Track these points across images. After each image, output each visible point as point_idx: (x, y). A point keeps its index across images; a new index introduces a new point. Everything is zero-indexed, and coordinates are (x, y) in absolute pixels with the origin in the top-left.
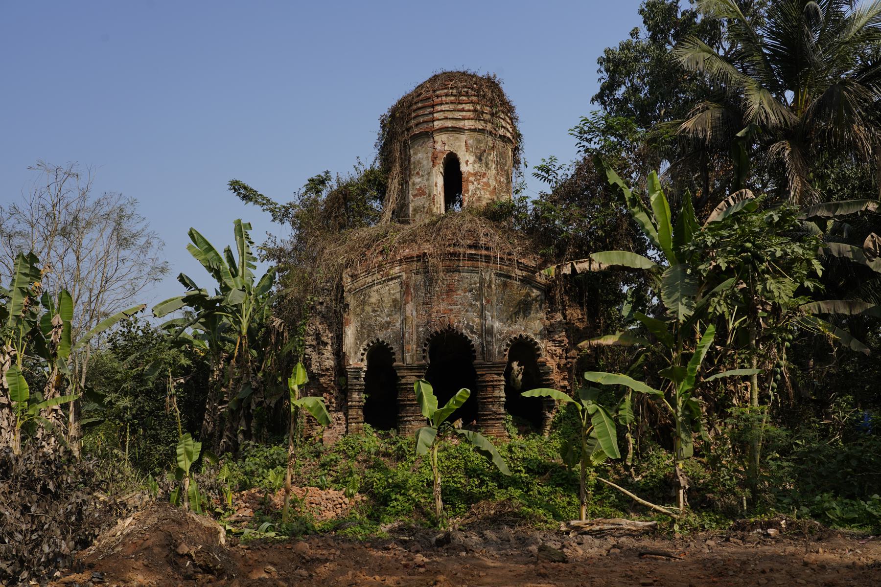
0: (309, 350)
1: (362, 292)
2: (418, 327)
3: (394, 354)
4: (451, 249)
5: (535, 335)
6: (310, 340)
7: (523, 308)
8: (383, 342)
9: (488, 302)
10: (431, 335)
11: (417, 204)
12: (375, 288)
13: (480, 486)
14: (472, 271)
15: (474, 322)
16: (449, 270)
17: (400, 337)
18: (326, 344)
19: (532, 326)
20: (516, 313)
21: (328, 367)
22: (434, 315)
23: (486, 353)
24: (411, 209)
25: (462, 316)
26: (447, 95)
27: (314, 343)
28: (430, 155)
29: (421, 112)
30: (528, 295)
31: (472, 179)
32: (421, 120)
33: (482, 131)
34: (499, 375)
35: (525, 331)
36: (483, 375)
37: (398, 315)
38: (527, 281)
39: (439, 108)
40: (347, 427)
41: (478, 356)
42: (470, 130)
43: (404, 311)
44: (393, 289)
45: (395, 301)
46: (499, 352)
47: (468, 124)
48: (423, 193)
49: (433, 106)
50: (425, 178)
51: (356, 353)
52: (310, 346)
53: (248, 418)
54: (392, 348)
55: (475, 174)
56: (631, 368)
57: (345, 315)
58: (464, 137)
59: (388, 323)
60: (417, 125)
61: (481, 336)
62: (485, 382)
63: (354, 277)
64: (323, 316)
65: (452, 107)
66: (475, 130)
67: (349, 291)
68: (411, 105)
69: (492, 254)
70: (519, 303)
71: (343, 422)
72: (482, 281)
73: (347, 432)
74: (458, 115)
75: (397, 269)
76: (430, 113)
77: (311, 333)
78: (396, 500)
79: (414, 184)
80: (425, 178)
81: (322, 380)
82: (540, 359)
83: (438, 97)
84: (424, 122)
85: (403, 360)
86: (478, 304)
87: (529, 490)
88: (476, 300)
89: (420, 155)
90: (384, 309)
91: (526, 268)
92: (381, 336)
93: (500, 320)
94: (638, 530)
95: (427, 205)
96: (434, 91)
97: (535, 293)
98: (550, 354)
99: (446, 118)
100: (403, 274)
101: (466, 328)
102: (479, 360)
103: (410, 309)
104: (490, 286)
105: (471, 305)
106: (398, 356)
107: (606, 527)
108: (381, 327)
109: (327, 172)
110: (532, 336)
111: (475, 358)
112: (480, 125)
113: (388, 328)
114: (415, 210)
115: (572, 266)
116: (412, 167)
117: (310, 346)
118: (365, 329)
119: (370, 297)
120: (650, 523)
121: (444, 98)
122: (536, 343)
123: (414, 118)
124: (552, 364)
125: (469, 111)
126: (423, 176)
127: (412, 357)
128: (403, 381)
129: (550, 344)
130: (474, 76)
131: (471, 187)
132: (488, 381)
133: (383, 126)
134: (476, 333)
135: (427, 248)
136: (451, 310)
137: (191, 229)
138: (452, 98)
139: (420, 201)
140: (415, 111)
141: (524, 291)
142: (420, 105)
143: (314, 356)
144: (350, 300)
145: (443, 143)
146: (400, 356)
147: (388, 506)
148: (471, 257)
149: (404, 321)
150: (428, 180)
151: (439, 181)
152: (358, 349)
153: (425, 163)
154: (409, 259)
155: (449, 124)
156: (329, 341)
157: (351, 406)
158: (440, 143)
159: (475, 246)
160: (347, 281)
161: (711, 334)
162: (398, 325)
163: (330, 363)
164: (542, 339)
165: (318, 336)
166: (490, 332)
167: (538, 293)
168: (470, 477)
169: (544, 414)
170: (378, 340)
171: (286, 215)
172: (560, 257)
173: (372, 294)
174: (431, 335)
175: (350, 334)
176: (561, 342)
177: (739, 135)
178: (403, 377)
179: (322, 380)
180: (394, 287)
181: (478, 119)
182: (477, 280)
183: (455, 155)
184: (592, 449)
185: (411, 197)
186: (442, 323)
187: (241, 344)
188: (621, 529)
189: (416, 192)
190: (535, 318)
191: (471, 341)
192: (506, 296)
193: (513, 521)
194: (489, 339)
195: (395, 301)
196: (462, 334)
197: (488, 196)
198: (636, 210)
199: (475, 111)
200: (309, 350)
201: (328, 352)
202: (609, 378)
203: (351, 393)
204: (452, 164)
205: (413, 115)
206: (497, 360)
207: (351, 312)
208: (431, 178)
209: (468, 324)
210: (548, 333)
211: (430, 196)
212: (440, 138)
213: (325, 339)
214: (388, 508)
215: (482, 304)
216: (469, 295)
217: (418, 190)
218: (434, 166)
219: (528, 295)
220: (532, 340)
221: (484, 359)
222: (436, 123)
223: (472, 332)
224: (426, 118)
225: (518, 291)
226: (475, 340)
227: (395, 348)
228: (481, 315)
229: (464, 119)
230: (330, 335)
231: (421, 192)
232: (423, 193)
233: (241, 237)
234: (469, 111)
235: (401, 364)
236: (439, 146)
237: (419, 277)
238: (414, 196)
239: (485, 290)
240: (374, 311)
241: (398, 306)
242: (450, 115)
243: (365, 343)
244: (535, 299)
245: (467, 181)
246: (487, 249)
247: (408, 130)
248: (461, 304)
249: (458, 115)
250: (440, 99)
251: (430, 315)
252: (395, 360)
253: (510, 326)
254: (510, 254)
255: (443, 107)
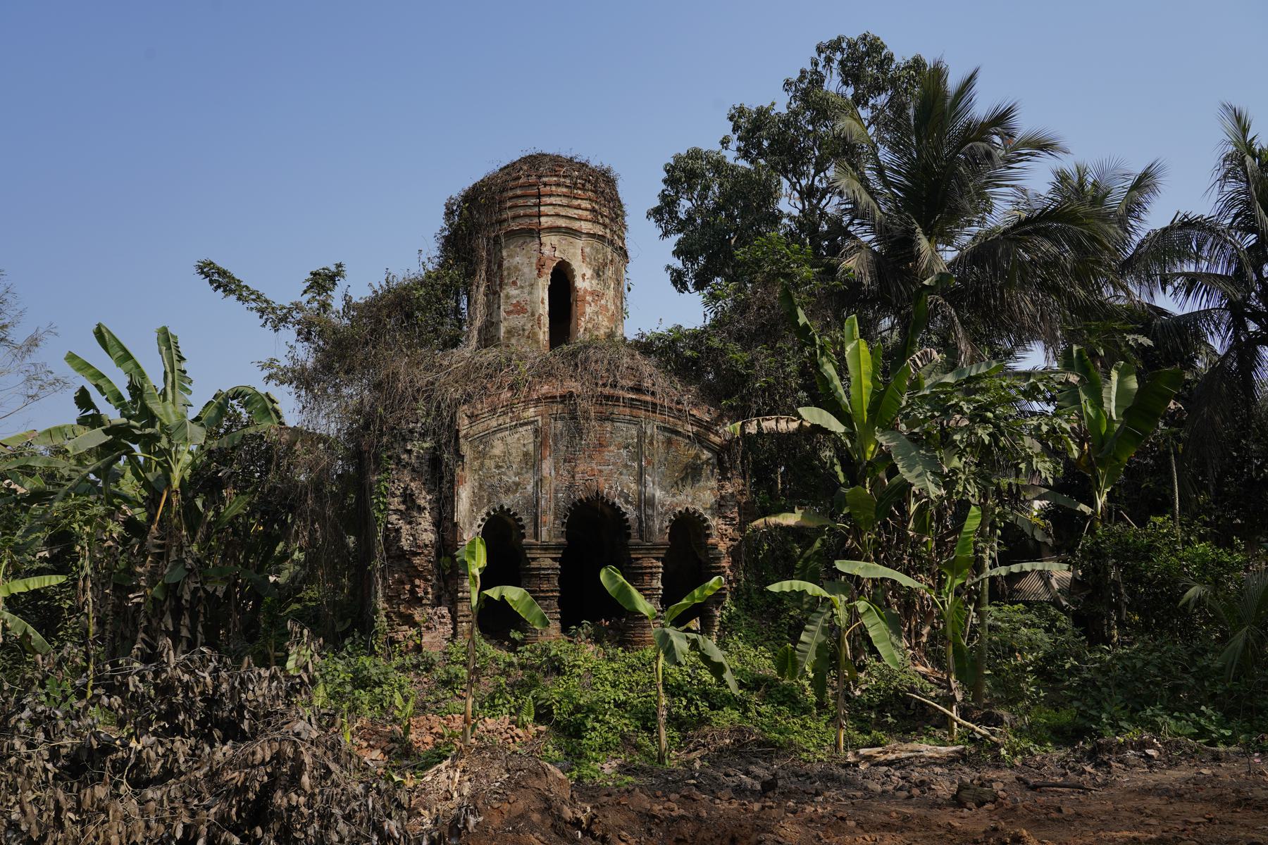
0: (393, 518)
1: (485, 438)
2: (556, 491)
3: (523, 527)
4: (607, 391)
5: (705, 509)
6: (395, 503)
7: (692, 473)
8: (509, 510)
9: (649, 463)
10: (574, 504)
11: (512, 324)
12: (499, 435)
13: (686, 707)
14: (629, 422)
15: (629, 488)
16: (603, 418)
17: (534, 505)
18: (421, 509)
19: (701, 497)
20: (682, 479)
21: (427, 542)
22: (578, 476)
23: (644, 531)
24: (503, 330)
25: (613, 478)
26: (558, 185)
27: (402, 507)
28: (534, 261)
29: (521, 202)
30: (697, 457)
31: (589, 298)
32: (522, 212)
33: (601, 238)
34: (657, 559)
35: (692, 503)
36: (638, 559)
37: (530, 474)
38: (700, 440)
39: (548, 200)
40: (454, 628)
41: (634, 534)
42: (588, 234)
43: (539, 469)
44: (523, 439)
45: (526, 454)
46: (661, 530)
47: (586, 227)
48: (523, 311)
49: (539, 196)
50: (526, 290)
51: (471, 525)
52: (396, 511)
53: (177, 614)
54: (520, 519)
55: (592, 293)
56: (805, 555)
57: (458, 471)
58: (580, 243)
59: (517, 484)
60: (514, 218)
61: (638, 507)
62: (641, 568)
63: (473, 417)
64: (413, 470)
65: (565, 201)
66: (593, 236)
67: (466, 437)
68: (504, 190)
69: (658, 402)
70: (686, 468)
71: (448, 620)
72: (641, 435)
73: (455, 635)
74: (571, 212)
75: (531, 411)
76: (535, 205)
77: (398, 493)
78: (594, 729)
79: (508, 297)
80: (526, 290)
81: (416, 561)
82: (711, 541)
83: (545, 185)
84: (525, 216)
85: (536, 536)
86: (635, 465)
87: (747, 710)
88: (634, 460)
89: (519, 259)
90: (509, 464)
91: (698, 422)
92: (507, 501)
93: (663, 488)
94: (941, 758)
95: (528, 326)
96: (540, 177)
97: (706, 455)
98: (721, 533)
99: (557, 215)
100: (539, 418)
101: (620, 495)
102: (634, 539)
103: (547, 467)
104: (651, 443)
105: (626, 466)
106: (529, 531)
107: (903, 755)
108: (508, 491)
109: (339, 266)
110: (701, 511)
111: (629, 536)
112: (599, 230)
113: (516, 491)
114: (510, 332)
115: (759, 424)
116: (505, 273)
117: (396, 511)
118: (485, 491)
119: (492, 447)
120: (954, 748)
121: (554, 188)
122: (705, 520)
123: (510, 208)
124: (723, 547)
125: (586, 209)
126: (522, 287)
127: (549, 531)
128: (534, 565)
129: (721, 521)
130: (583, 165)
131: (589, 310)
132: (646, 568)
133: (449, 213)
134: (631, 504)
135: (574, 386)
136: (601, 471)
137: (99, 326)
138: (565, 190)
139: (517, 321)
140: (511, 198)
141: (692, 452)
142: (519, 192)
143: (405, 529)
144: (466, 449)
145: (554, 247)
146: (532, 531)
147: (582, 738)
148: (631, 404)
149: (539, 483)
150: (530, 293)
151: (543, 293)
152: (475, 518)
153: (526, 270)
154: (551, 399)
155: (562, 223)
156: (428, 507)
157: (462, 598)
158: (549, 247)
159: (637, 389)
160: (464, 424)
161: (976, 517)
162: (530, 488)
163: (429, 537)
164: (713, 514)
165: (408, 498)
166: (650, 502)
167: (710, 455)
168: (673, 695)
169: (711, 611)
170: (502, 507)
171: (284, 319)
172: (742, 414)
173: (496, 443)
174: (574, 504)
175: (464, 496)
176: (733, 519)
177: (926, 282)
178: (534, 559)
179: (416, 561)
180: (526, 433)
181: (595, 222)
182: (635, 433)
183: (569, 265)
184: (805, 657)
185: (503, 314)
186: (588, 488)
187: (168, 500)
188: (921, 757)
189: (511, 308)
190: (706, 488)
191: (625, 514)
192: (670, 457)
193: (769, 752)
194: (650, 512)
195: (526, 454)
196: (614, 504)
197: (606, 323)
198: (824, 359)
199: (593, 210)
200: (393, 518)
201: (426, 521)
202: (867, 568)
203: (462, 580)
204: (562, 280)
205: (509, 204)
206: (658, 541)
207: (467, 467)
208: (535, 291)
209: (622, 491)
210: (719, 508)
211: (533, 315)
212: (549, 240)
213: (422, 502)
214: (584, 741)
215: (640, 466)
216: (624, 452)
217: (515, 306)
218: (539, 275)
219: (697, 457)
220: (701, 515)
221: (641, 537)
222: (543, 219)
223: (627, 502)
224: (529, 211)
225: (686, 452)
226: (631, 513)
227: (526, 519)
228: (640, 480)
229: (580, 219)
230: (428, 497)
231: (519, 309)
232: (523, 311)
233: (169, 348)
234: (586, 209)
235: (533, 541)
236: (547, 251)
237: (560, 424)
238: (508, 313)
239: (645, 447)
240: (498, 467)
241: (532, 462)
242: (563, 212)
243: (485, 510)
244: (707, 462)
245: (584, 300)
246: (653, 394)
247: (501, 222)
248: (614, 464)
249: (571, 212)
250: (548, 188)
251: (573, 477)
252: (524, 536)
253: (674, 496)
254: (678, 403)
255: (553, 200)
